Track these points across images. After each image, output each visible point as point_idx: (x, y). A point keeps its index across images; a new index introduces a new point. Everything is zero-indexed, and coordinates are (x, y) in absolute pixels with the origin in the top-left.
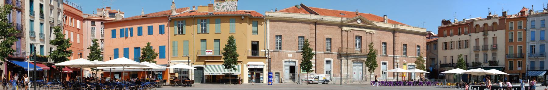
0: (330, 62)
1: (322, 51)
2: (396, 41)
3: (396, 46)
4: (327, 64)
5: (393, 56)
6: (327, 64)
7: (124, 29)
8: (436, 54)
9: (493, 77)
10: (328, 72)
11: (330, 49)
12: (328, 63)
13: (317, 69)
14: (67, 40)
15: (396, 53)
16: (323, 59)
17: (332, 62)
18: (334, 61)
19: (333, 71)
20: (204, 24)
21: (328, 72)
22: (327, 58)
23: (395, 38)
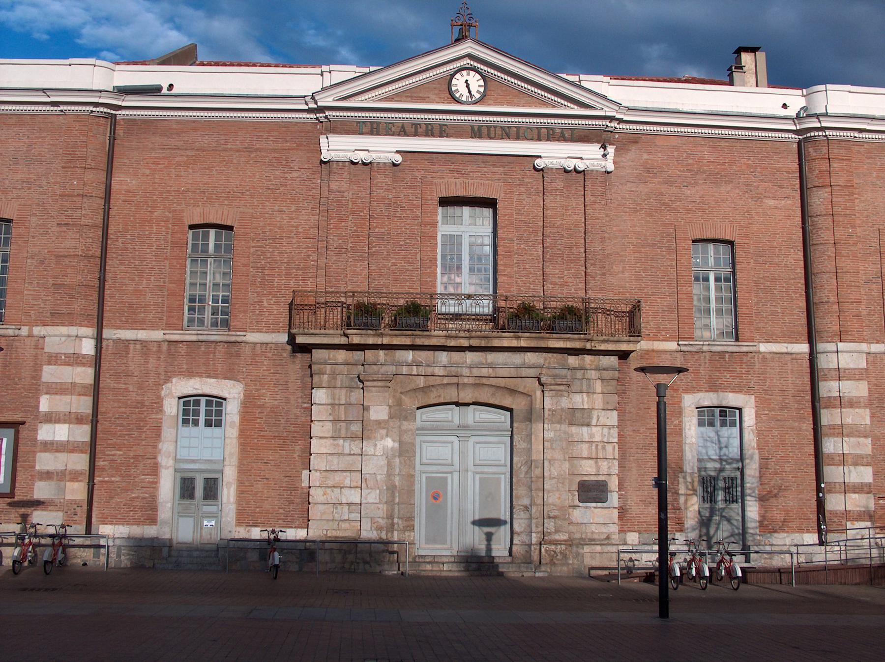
0: (216, 402)
1: (153, 327)
2: (823, 222)
3: (823, 263)
4: (196, 423)
5: (804, 348)
6: (196, 423)
7: (735, 417)
8: (560, 139)
9: (194, 291)
10: (199, 491)
11: (224, 313)
12: (202, 418)
13: (100, 463)
14: (39, 398)
15: (827, 322)
16: (159, 385)
17: (232, 411)
18: (249, 405)
19: (240, 482)
20: (197, 300)
21: (199, 491)
22: (190, 374)
23: (819, 200)
